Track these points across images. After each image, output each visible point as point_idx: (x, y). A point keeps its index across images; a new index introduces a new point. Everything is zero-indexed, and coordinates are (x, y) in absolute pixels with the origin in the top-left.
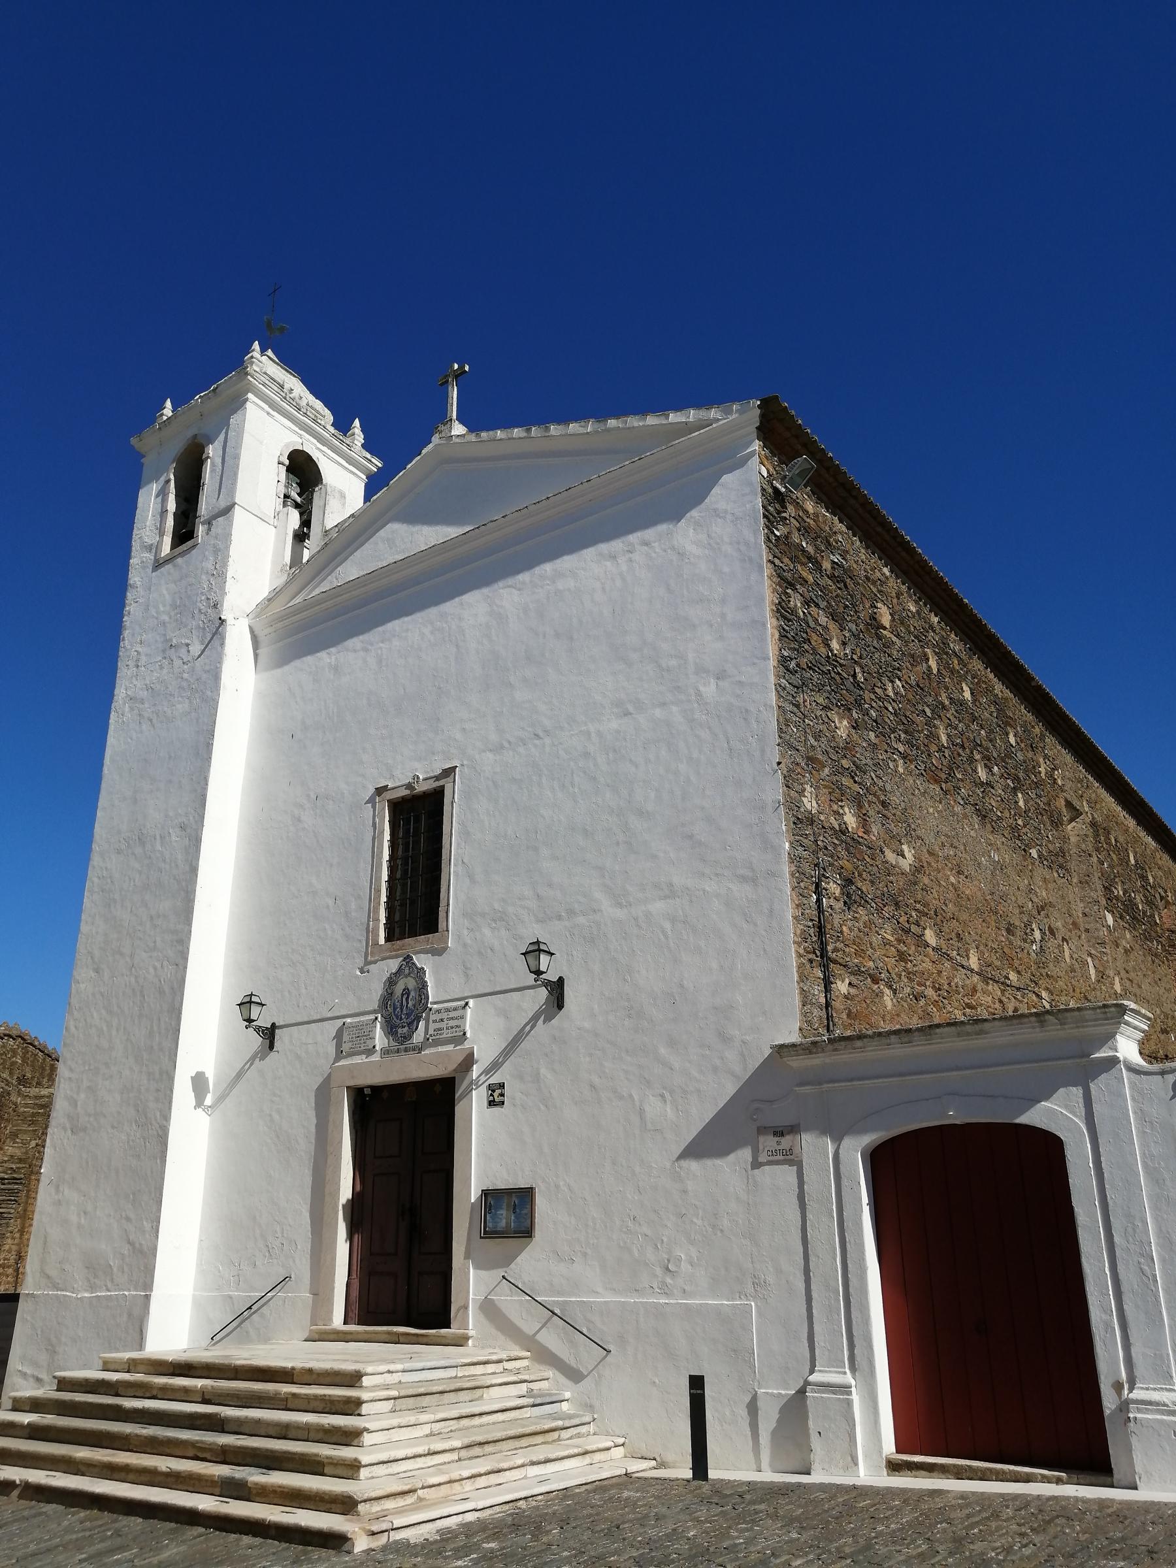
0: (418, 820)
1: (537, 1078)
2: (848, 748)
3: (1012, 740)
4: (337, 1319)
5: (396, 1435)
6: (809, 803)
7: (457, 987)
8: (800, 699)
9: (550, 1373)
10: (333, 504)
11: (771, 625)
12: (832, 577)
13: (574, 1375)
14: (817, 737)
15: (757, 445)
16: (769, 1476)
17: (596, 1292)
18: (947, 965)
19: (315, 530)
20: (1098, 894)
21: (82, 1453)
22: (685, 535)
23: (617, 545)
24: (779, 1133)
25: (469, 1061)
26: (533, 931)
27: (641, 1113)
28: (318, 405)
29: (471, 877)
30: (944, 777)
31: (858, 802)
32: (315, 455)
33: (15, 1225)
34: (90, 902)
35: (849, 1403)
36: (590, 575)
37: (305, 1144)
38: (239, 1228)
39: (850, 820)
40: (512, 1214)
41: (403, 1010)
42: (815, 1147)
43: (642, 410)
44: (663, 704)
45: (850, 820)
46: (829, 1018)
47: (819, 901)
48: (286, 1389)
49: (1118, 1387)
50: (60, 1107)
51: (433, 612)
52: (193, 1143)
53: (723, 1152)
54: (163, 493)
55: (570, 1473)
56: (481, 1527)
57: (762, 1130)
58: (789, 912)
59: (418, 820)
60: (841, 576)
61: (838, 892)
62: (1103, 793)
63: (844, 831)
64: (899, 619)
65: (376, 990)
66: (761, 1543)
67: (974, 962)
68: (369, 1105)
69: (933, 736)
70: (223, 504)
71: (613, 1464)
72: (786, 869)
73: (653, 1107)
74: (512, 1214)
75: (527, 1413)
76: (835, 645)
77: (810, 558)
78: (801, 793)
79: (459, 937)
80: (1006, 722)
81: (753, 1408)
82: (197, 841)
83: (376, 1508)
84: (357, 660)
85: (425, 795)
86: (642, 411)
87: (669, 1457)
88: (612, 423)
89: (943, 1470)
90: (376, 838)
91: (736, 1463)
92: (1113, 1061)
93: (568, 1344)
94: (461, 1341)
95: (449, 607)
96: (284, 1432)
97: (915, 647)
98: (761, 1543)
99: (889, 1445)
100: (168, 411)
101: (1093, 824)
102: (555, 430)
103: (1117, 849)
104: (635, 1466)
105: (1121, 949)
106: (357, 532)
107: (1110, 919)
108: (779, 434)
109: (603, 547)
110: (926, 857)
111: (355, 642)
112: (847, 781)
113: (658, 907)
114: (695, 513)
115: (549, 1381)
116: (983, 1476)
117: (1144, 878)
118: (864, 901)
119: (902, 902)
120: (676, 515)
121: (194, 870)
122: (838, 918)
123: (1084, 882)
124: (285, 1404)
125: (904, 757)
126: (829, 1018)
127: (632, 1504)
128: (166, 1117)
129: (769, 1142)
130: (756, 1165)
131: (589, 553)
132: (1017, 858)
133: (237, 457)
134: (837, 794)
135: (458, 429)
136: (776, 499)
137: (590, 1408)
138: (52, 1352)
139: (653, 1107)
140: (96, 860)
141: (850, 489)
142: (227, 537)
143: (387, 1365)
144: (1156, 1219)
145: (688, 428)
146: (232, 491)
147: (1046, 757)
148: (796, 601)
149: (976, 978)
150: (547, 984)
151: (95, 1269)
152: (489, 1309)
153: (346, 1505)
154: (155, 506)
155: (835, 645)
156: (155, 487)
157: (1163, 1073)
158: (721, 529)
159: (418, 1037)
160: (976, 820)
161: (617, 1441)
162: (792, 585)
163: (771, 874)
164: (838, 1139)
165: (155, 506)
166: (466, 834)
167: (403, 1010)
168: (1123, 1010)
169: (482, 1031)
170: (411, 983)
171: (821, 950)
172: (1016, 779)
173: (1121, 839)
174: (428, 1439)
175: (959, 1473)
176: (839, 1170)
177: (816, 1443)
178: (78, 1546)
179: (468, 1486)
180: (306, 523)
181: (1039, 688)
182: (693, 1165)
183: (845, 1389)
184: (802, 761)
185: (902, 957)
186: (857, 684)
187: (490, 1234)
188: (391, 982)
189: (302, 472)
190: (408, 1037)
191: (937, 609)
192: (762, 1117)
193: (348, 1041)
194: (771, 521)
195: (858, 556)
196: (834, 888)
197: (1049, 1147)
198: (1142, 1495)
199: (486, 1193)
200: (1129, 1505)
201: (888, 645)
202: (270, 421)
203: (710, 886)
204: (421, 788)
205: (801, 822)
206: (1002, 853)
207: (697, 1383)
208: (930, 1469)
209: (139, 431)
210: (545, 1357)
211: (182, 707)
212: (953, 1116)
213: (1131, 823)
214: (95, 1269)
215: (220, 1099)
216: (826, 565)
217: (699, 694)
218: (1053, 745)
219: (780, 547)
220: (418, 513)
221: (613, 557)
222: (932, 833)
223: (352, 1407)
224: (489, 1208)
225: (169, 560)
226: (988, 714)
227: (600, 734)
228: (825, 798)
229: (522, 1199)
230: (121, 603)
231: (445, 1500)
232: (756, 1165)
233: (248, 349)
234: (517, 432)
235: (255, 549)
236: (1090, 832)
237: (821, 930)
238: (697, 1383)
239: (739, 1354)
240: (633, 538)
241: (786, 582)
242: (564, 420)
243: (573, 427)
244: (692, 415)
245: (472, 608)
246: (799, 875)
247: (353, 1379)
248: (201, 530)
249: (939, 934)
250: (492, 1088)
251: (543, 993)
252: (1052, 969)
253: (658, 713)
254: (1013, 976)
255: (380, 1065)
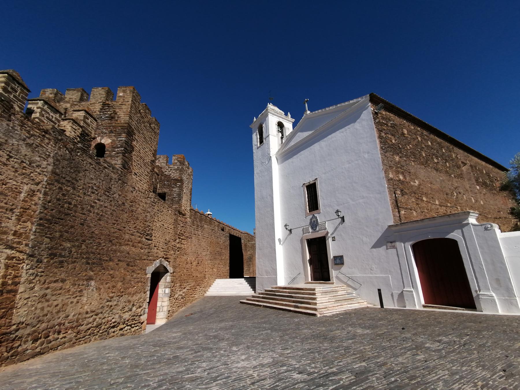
0: (312, 189)
1: (341, 235)
2: (399, 162)
3: (444, 151)
4: (310, 280)
5: (323, 299)
6: (391, 176)
7: (324, 220)
8: (386, 155)
9: (350, 289)
10: (287, 131)
11: (378, 141)
12: (391, 127)
13: (355, 289)
14: (391, 162)
15: (370, 104)
16: (397, 308)
17: (357, 274)
18: (430, 204)
19: (284, 136)
20: (474, 181)
21: (271, 301)
22: (357, 125)
23: (343, 130)
24: (391, 243)
25: (328, 233)
26: (337, 208)
27: (362, 241)
28: (281, 111)
29: (323, 199)
30: (425, 163)
31: (403, 173)
32: (282, 121)
33: (252, 266)
34: (256, 210)
35: (413, 294)
36: (338, 136)
37: (300, 250)
38: (290, 265)
39: (401, 177)
40: (339, 260)
41: (314, 224)
42: (400, 245)
43: (344, 101)
44: (357, 160)
45: (401, 177)
46: (400, 219)
47: (395, 196)
48: (302, 291)
49: (476, 291)
50: (257, 245)
51: (309, 148)
52: (280, 251)
53: (380, 247)
54: (256, 135)
55: (355, 306)
56: (340, 314)
57: (388, 242)
58: (389, 199)
59: (312, 189)
60: (394, 126)
61: (400, 193)
62: (473, 158)
63: (400, 180)
64: (409, 131)
65: (309, 221)
66: (393, 318)
67: (437, 203)
68: (310, 242)
69: (421, 155)
70: (267, 135)
71: (365, 305)
72: (387, 190)
73: (365, 239)
74: (339, 260)
75: (347, 296)
76: (393, 141)
77: (385, 124)
78: (389, 174)
79: (322, 210)
80: (442, 147)
81: (392, 295)
82: (272, 198)
83: (321, 310)
84: (295, 160)
85: (312, 184)
86: (344, 102)
87: (376, 304)
88: (338, 105)
89: (436, 307)
90: (304, 193)
91: (389, 305)
92: (468, 224)
93: (353, 284)
94: (333, 283)
95: (311, 147)
96: (303, 298)
97: (414, 136)
98: (393, 318)
99: (423, 302)
100: (255, 119)
101: (471, 166)
102: (327, 109)
103: (479, 170)
104: (369, 305)
105: (482, 194)
106: (292, 135)
107: (478, 187)
108: (374, 100)
109: (340, 130)
110: (422, 182)
111: (295, 157)
112: (399, 169)
113: (361, 201)
114: (358, 120)
115: (350, 290)
116: (445, 308)
117: (489, 176)
118: (406, 194)
119: (417, 193)
120: (354, 121)
121: (273, 203)
122: (400, 198)
123: (469, 180)
124: (303, 294)
125: (414, 161)
126: (400, 219)
127: (368, 311)
128: (275, 246)
129: (389, 244)
130: (387, 249)
131: (338, 132)
132: (448, 178)
133: (268, 126)
134: (397, 172)
135: (308, 112)
136: (376, 114)
137: (359, 295)
138: (262, 286)
139: (365, 239)
140: (256, 203)
141: (393, 107)
142: (269, 141)
143: (319, 288)
144: (483, 257)
145: (354, 103)
146: (269, 133)
147: (454, 153)
148: (383, 134)
149: (438, 206)
150: (341, 217)
151: (267, 272)
152: (337, 277)
153: (315, 309)
154: (256, 137)
155: (393, 141)
156: (255, 134)
157: (481, 225)
158: (364, 123)
159: (318, 229)
160: (435, 172)
161: (365, 301)
162: (382, 131)
163: (384, 192)
164: (404, 243)
165: (256, 137)
166: (321, 190)
167: (314, 224)
168: (469, 213)
169: (330, 227)
170: (315, 220)
171: (397, 205)
172: (446, 160)
173: (480, 168)
174: (329, 300)
175: (439, 308)
176: (406, 250)
177: (406, 301)
178: (273, 314)
179: (337, 307)
180: (283, 135)
181: (450, 137)
182: (374, 250)
183: (412, 291)
184: (388, 167)
185: (417, 204)
186: (400, 148)
187: (336, 264)
188: (311, 219)
189: (280, 125)
190: (315, 229)
191: (419, 126)
192: (388, 239)
193: (305, 231)
194: (375, 119)
195: (397, 120)
196: (399, 192)
197: (454, 243)
198: (484, 313)
199: (334, 257)
200: (479, 315)
201: (407, 138)
202: (274, 116)
203: (371, 196)
204: (311, 183)
205: (389, 180)
206: (443, 177)
207: (379, 290)
208: (433, 307)
209: (250, 124)
210: (349, 286)
211: (266, 173)
212: (430, 237)
213: (484, 163)
214: (267, 272)
215: (283, 243)
216: (389, 125)
217: (364, 157)
218: (456, 150)
219: (378, 124)
220: (302, 131)
221: (343, 132)
222: (422, 176)
223: (315, 299)
224: (335, 260)
225: (260, 147)
226: (436, 146)
227: (345, 168)
228: (394, 173)
229: (341, 257)
230: (253, 156)
231: (333, 309)
232: (387, 249)
233: (267, 105)
234: (320, 111)
235: (274, 142)
236: (470, 168)
237: (396, 201)
238: (379, 290)
239: (388, 285)
240: (346, 128)
241: (380, 131)
242: (329, 106)
243: (331, 108)
244: (355, 100)
245: (316, 147)
246: (390, 191)
247: (314, 290)
248: (264, 140)
249: (427, 197)
250: (333, 238)
251: (340, 219)
252: (461, 202)
253: (356, 162)
254: (449, 205)
255: (311, 235)
